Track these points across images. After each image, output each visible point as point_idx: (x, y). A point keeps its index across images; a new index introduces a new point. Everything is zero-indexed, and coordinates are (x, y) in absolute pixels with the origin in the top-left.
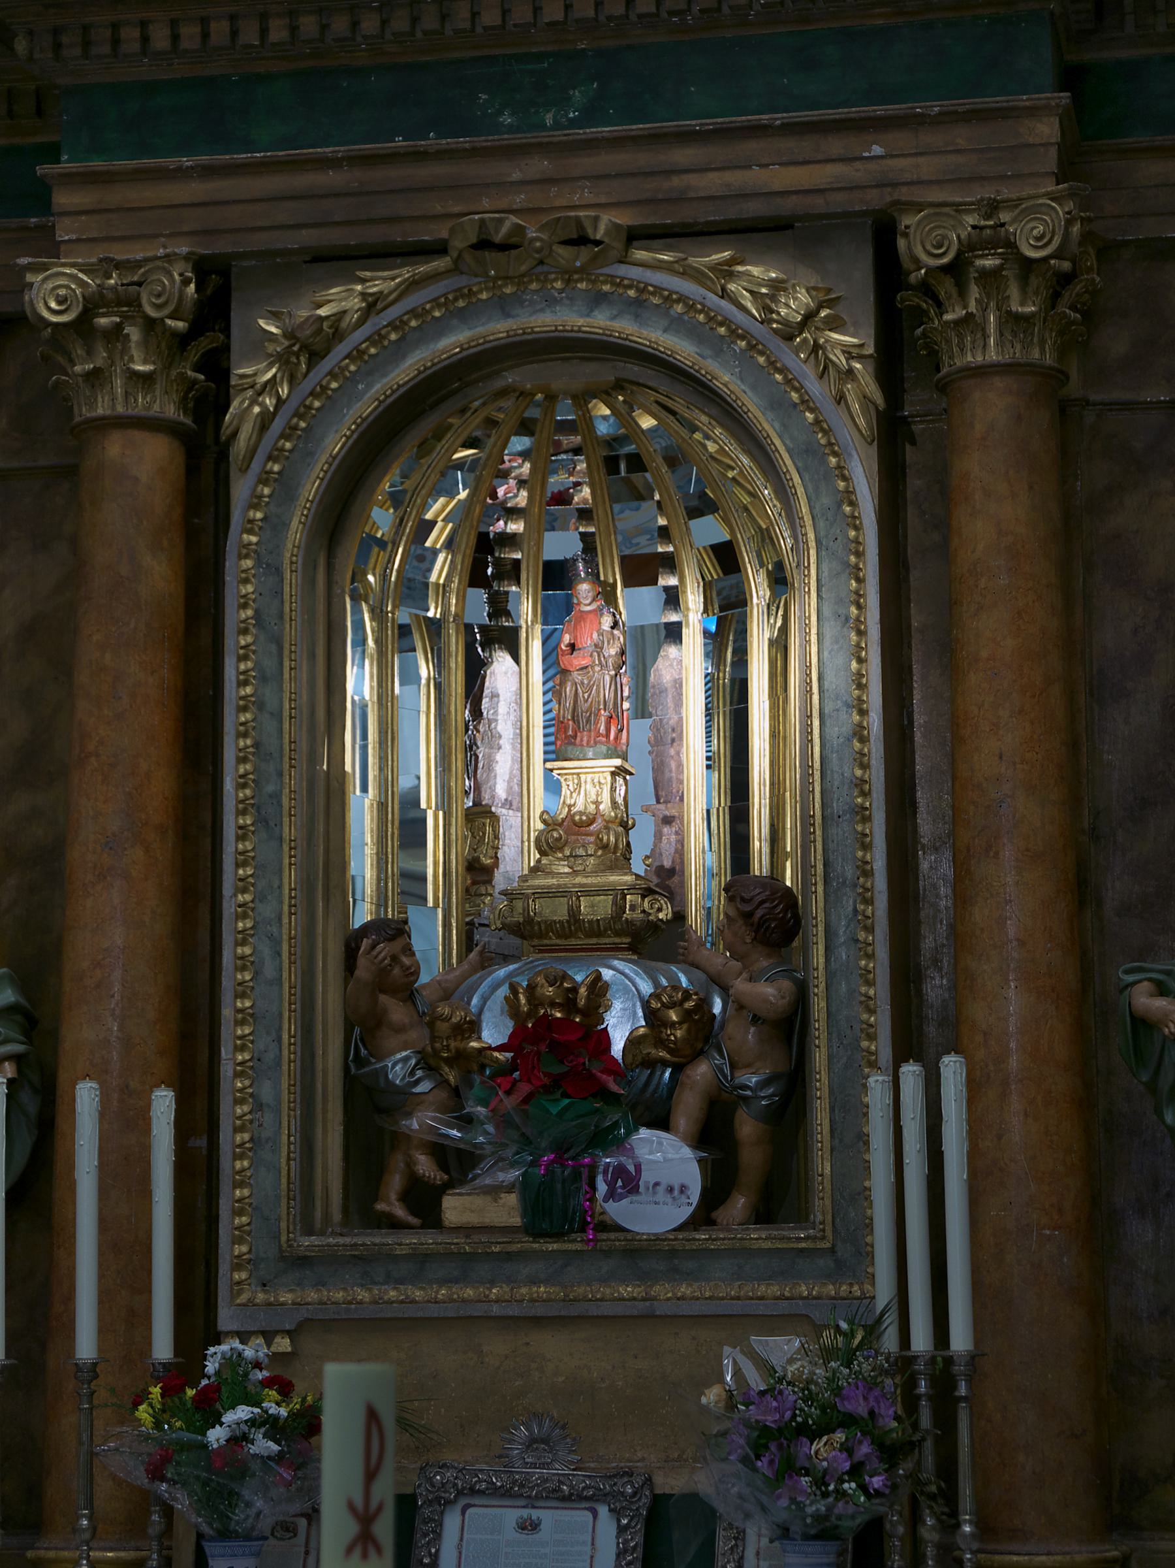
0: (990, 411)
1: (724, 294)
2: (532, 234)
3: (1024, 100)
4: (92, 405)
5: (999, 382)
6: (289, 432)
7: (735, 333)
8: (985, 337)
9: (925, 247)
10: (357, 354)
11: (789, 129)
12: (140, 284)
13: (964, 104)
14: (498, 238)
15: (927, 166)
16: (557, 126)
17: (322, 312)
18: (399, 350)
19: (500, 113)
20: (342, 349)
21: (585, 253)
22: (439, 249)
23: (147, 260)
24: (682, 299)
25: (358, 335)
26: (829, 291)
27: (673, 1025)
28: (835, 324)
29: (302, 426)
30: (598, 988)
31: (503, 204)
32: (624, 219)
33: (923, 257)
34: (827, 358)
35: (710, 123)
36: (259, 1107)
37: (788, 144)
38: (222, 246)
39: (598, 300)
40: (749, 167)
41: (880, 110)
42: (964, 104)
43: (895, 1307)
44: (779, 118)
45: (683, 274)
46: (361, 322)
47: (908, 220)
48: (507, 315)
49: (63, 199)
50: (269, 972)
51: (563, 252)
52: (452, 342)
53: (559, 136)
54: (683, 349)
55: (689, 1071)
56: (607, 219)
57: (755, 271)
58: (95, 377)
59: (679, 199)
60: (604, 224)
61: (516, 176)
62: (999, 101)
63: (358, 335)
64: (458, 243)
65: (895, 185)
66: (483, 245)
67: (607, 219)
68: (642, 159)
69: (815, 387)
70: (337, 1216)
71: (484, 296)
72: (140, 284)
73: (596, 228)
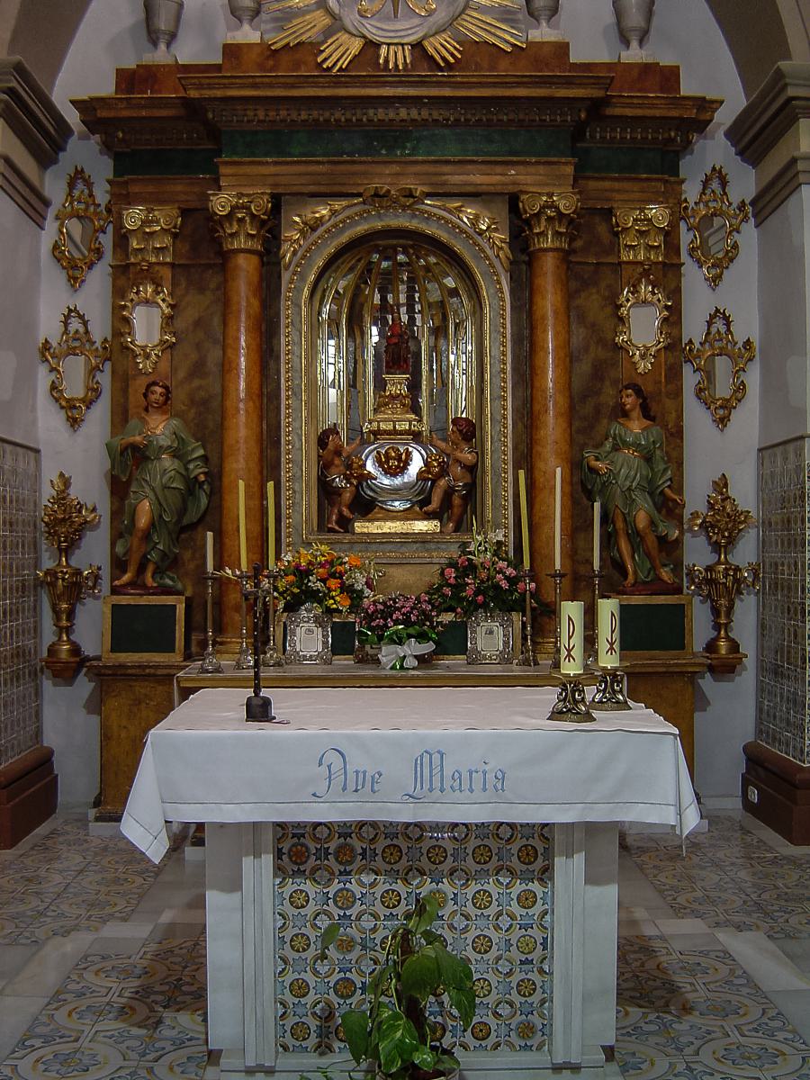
0: (549, 264)
1: (459, 218)
2: (392, 192)
3: (563, 160)
4: (232, 244)
5: (551, 254)
6: (304, 257)
7: (463, 231)
8: (547, 239)
9: (531, 206)
10: (328, 231)
11: (483, 162)
12: (251, 202)
13: (545, 159)
14: (381, 193)
15: (529, 179)
16: (402, 155)
17: (317, 215)
18: (342, 231)
19: (381, 149)
20: (321, 230)
21: (411, 200)
22: (359, 195)
23: (254, 194)
24: (443, 218)
25: (329, 224)
26: (494, 219)
27: (435, 467)
28: (496, 230)
29: (308, 255)
30: (409, 454)
31: (383, 181)
32: (426, 189)
33: (528, 210)
34: (494, 243)
35: (457, 158)
36: (294, 492)
37: (483, 167)
38: (280, 190)
39: (414, 216)
40: (469, 175)
41: (515, 159)
42: (545, 159)
43: (36, 182)
44: (481, 159)
45: (444, 210)
46: (329, 220)
47: (524, 197)
48: (381, 220)
49: (224, 170)
50: (297, 445)
51: (403, 199)
52: (361, 229)
53: (403, 159)
54: (444, 236)
55: (438, 482)
56: (420, 189)
57: (469, 211)
58: (233, 235)
59: (444, 184)
60: (419, 190)
61: (387, 172)
62: (555, 159)
63: (329, 224)
64: (367, 194)
65: (519, 184)
66: (376, 195)
67: (420, 189)
68: (431, 169)
69: (489, 252)
70: (316, 529)
71: (373, 213)
72: (251, 202)
73: (416, 192)
